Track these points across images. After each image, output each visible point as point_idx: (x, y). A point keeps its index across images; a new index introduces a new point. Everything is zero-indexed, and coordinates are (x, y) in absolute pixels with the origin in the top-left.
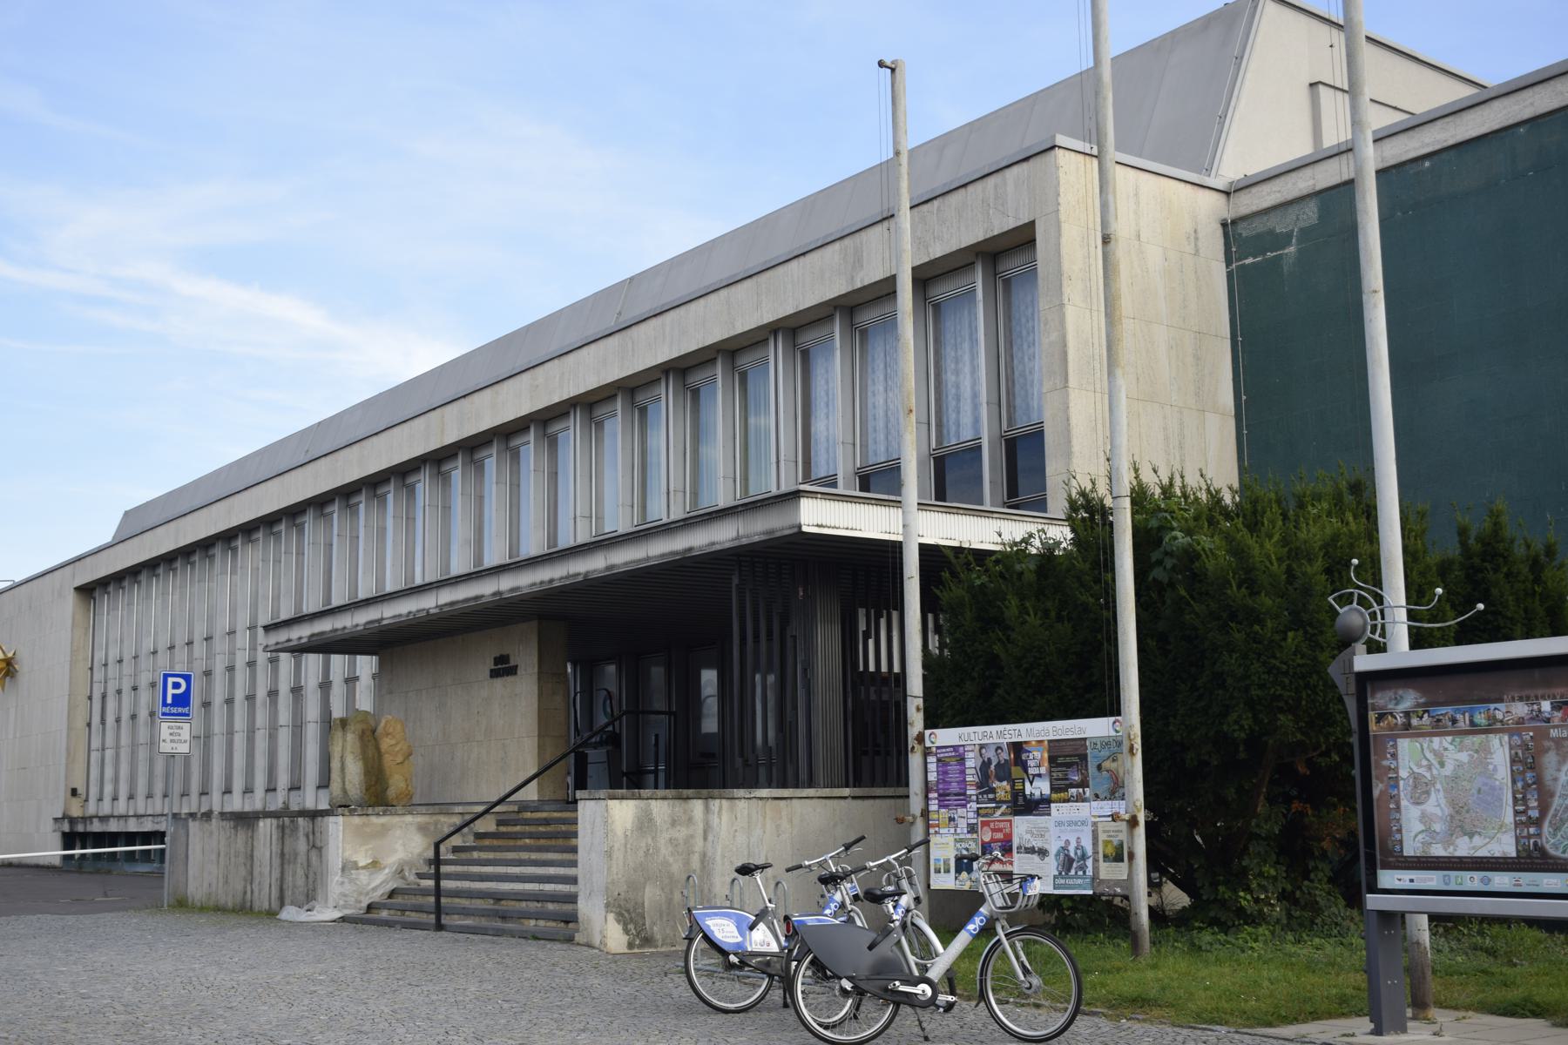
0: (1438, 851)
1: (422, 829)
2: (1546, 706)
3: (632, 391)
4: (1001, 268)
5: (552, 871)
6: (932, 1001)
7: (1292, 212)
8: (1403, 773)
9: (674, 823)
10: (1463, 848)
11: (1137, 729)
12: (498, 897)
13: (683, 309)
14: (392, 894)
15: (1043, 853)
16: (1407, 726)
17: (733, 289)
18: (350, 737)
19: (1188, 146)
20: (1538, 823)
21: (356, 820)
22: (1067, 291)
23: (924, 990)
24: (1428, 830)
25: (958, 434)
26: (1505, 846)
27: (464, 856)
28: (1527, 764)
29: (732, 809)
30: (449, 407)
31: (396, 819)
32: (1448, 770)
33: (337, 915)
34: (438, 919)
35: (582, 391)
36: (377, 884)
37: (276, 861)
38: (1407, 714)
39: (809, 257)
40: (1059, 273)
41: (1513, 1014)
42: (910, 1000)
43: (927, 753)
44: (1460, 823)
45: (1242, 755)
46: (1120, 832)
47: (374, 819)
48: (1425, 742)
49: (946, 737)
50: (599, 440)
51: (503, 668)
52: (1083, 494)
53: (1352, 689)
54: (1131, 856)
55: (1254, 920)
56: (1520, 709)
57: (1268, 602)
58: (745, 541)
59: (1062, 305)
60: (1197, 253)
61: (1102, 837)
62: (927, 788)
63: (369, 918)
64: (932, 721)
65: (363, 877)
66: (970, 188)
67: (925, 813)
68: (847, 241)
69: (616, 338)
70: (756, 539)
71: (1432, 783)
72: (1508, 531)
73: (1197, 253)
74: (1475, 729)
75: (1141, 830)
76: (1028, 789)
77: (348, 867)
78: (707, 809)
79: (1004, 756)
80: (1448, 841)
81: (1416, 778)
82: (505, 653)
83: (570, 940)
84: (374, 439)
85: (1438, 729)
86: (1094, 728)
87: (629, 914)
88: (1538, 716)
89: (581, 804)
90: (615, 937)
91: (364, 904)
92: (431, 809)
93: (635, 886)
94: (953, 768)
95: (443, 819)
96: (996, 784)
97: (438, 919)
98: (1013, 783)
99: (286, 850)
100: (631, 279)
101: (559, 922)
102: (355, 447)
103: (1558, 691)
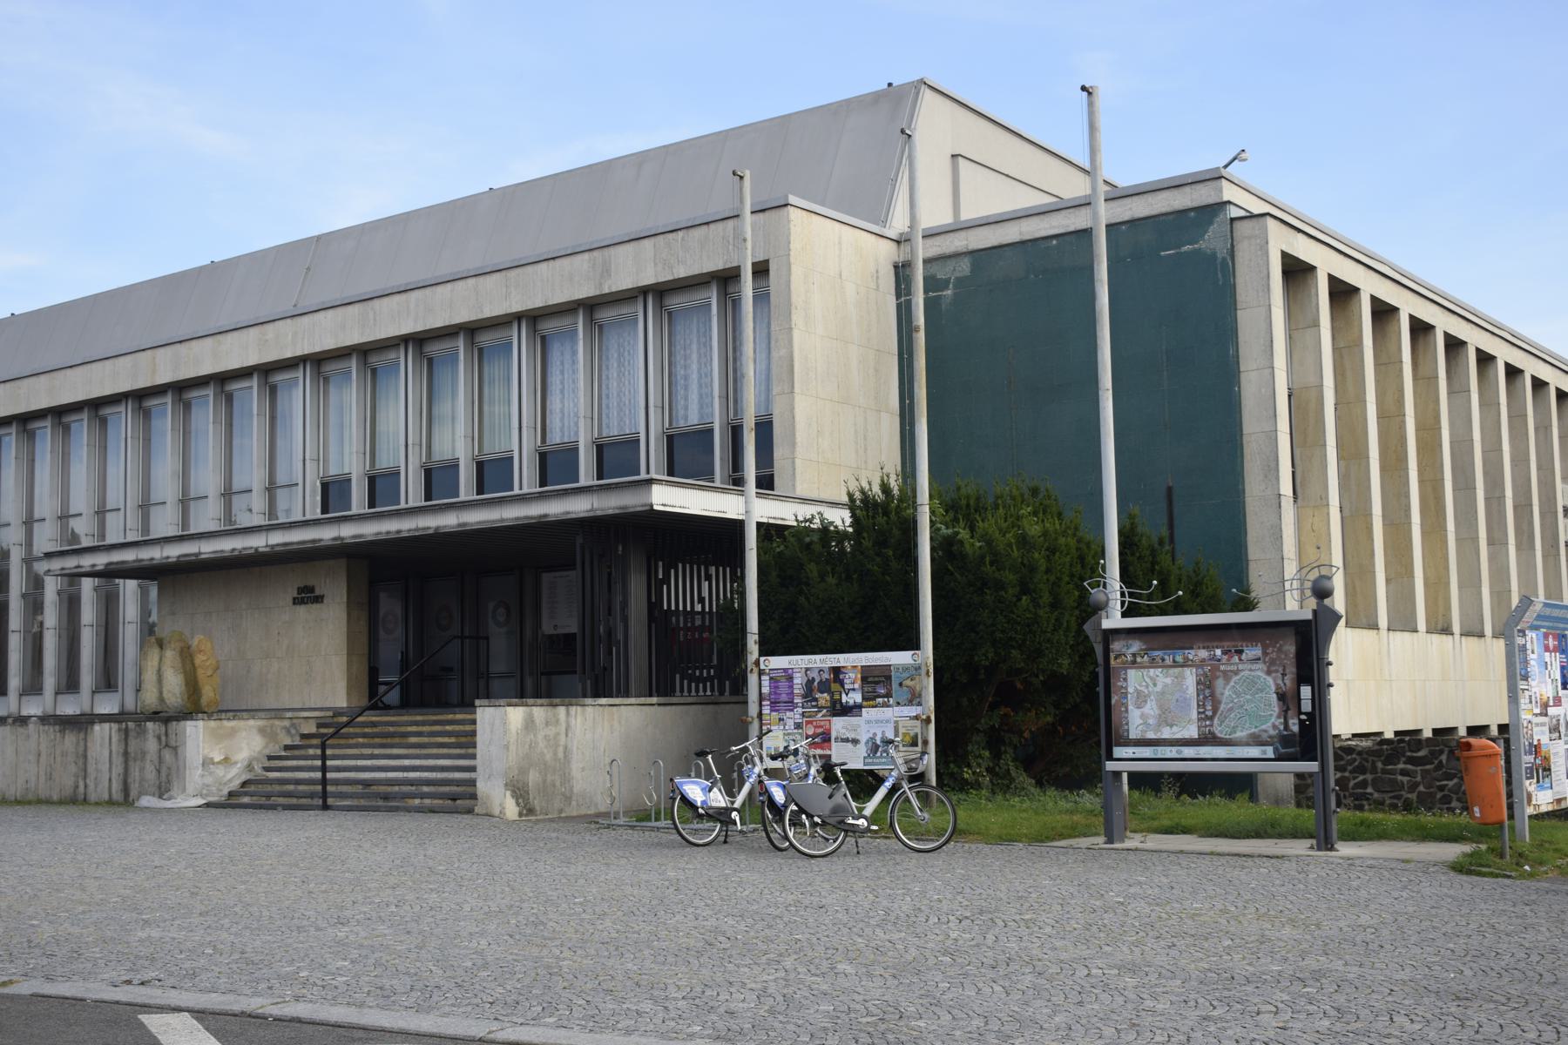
0: (1151, 735)
1: (262, 731)
2: (1218, 652)
3: (367, 355)
4: (731, 289)
5: (407, 762)
6: (868, 830)
7: (951, 264)
8: (1131, 690)
9: (547, 724)
10: (1166, 733)
11: (931, 660)
12: (367, 784)
13: (428, 291)
14: (244, 784)
15: (855, 742)
16: (1134, 662)
17: (481, 279)
18: (169, 654)
19: (864, 202)
20: (1211, 718)
21: (212, 724)
22: (794, 317)
23: (862, 822)
24: (1145, 723)
25: (686, 418)
26: (1192, 732)
27: (297, 753)
28: (1207, 687)
29: (583, 713)
30: (161, 350)
31: (242, 723)
32: (1159, 688)
33: (201, 801)
34: (325, 801)
35: (318, 349)
36: (233, 777)
37: (118, 761)
38: (1134, 655)
39: (558, 262)
40: (789, 304)
41: (1171, 833)
42: (853, 830)
43: (761, 673)
44: (1165, 719)
45: (982, 677)
46: (917, 728)
47: (225, 723)
48: (1145, 672)
49: (778, 662)
50: (326, 393)
51: (307, 596)
52: (862, 491)
53: (1099, 639)
54: (926, 743)
55: (977, 786)
56: (1203, 654)
57: (1011, 577)
58: (599, 513)
59: (791, 329)
60: (877, 289)
61: (902, 731)
62: (761, 698)
63: (232, 802)
64: (767, 649)
65: (220, 771)
66: (712, 226)
67: (760, 715)
68: (595, 253)
69: (357, 306)
70: (611, 512)
71: (1149, 695)
72: (1140, 529)
73: (877, 289)
74: (1175, 665)
75: (932, 726)
76: (844, 699)
77: (207, 762)
78: (568, 714)
79: (826, 676)
80: (1157, 731)
81: (1138, 692)
82: (310, 583)
83: (470, 811)
84: (69, 372)
85: (1153, 663)
86: (898, 658)
87: (519, 791)
88: (1213, 658)
89: (479, 710)
90: (511, 809)
91: (226, 791)
92: (269, 715)
93: (523, 771)
94: (783, 684)
95: (277, 722)
96: (818, 695)
97: (325, 801)
98: (832, 694)
99: (131, 749)
100: (319, 238)
101: (459, 799)
102: (42, 378)
103: (1226, 644)
